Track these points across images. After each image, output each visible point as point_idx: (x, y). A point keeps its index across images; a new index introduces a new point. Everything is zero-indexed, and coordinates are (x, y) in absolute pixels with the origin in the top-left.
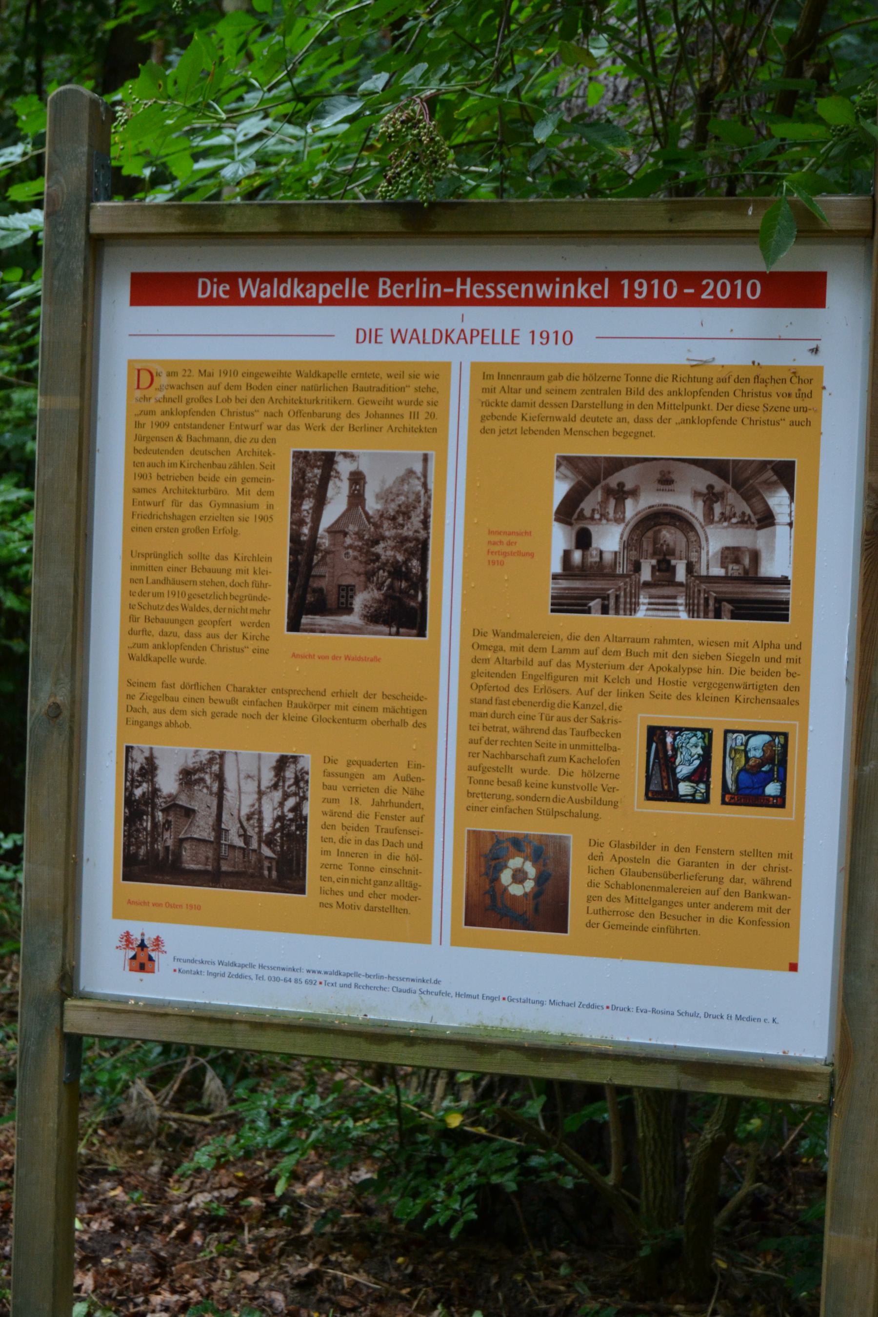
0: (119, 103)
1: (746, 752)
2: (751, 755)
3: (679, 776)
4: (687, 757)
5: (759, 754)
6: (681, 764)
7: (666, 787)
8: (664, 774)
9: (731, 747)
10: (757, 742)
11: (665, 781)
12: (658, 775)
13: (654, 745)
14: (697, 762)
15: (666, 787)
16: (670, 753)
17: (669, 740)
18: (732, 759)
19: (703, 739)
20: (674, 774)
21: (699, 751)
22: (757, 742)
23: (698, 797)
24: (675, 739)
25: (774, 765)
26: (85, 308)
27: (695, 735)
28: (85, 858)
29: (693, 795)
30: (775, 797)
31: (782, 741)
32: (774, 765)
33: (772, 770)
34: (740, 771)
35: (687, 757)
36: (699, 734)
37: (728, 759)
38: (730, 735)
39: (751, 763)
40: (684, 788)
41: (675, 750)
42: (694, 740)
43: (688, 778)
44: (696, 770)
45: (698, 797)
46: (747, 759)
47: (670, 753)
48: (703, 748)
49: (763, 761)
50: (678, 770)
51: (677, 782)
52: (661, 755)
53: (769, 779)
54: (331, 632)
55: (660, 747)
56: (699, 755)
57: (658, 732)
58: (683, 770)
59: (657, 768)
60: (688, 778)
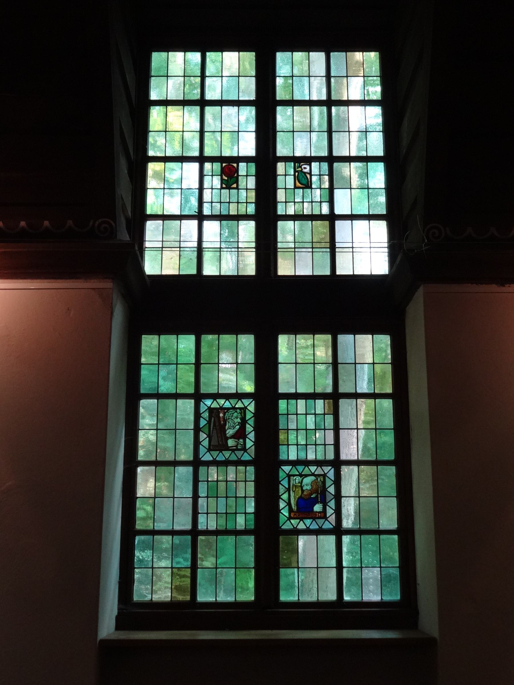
1: (302, 487)
2: (304, 488)
3: (228, 435)
4: (232, 424)
5: (309, 487)
6: (229, 428)
7: (220, 443)
8: (219, 435)
10: (308, 480)
11: (220, 439)
12: (216, 435)
13: (213, 419)
14: (238, 427)
15: (220, 443)
17: (221, 415)
19: (241, 413)
20: (225, 434)
21: (239, 420)
22: (308, 480)
24: (224, 414)
25: (318, 493)
27: (236, 412)
28: (362, 155)
29: (236, 446)
30: (319, 512)
31: (322, 479)
32: (318, 493)
33: (317, 497)
34: (299, 498)
35: (232, 424)
36: (238, 411)
38: (292, 477)
39: (305, 493)
40: (231, 443)
41: (225, 421)
43: (233, 437)
44: (237, 432)
45: (239, 447)
46: (303, 491)
47: (222, 422)
48: (241, 419)
49: (312, 492)
50: (227, 432)
51: (227, 439)
52: (217, 424)
53: (315, 502)
55: (216, 420)
56: (239, 423)
57: (215, 411)
58: (230, 432)
59: (215, 431)
60: (233, 437)
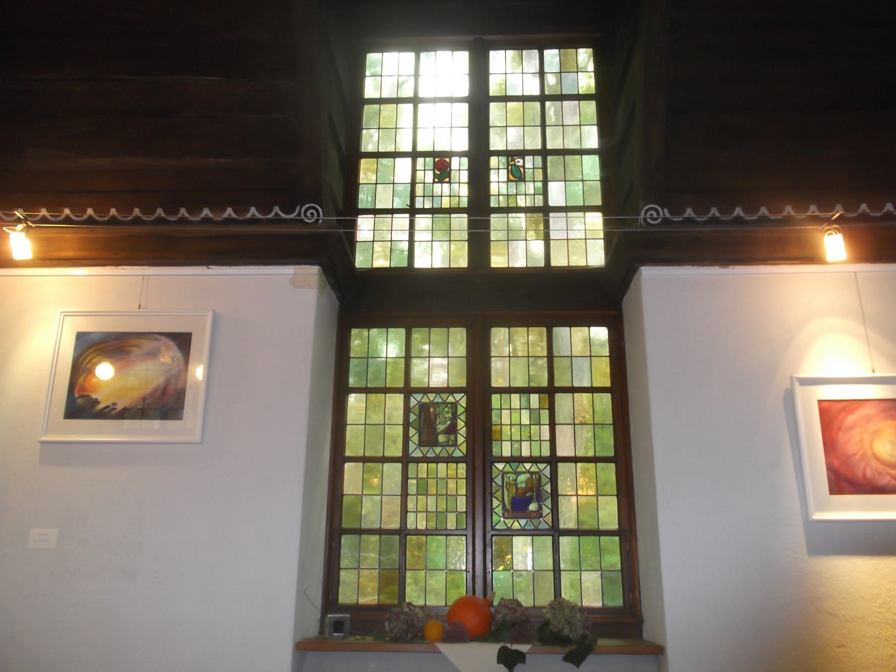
0: (407, 205)
1: (516, 485)
2: (519, 486)
3: (438, 431)
4: (443, 419)
6: (440, 423)
9: (507, 483)
14: (449, 422)
16: (433, 417)
18: (508, 490)
19: (452, 408)
21: (450, 415)
23: (450, 443)
26: (52, 260)
27: (447, 407)
29: (448, 442)
31: (537, 477)
35: (443, 419)
36: (449, 405)
37: (505, 490)
39: (520, 491)
40: (441, 438)
42: (446, 409)
46: (517, 489)
47: (433, 417)
54: (124, 414)
56: (450, 418)
58: (441, 427)
